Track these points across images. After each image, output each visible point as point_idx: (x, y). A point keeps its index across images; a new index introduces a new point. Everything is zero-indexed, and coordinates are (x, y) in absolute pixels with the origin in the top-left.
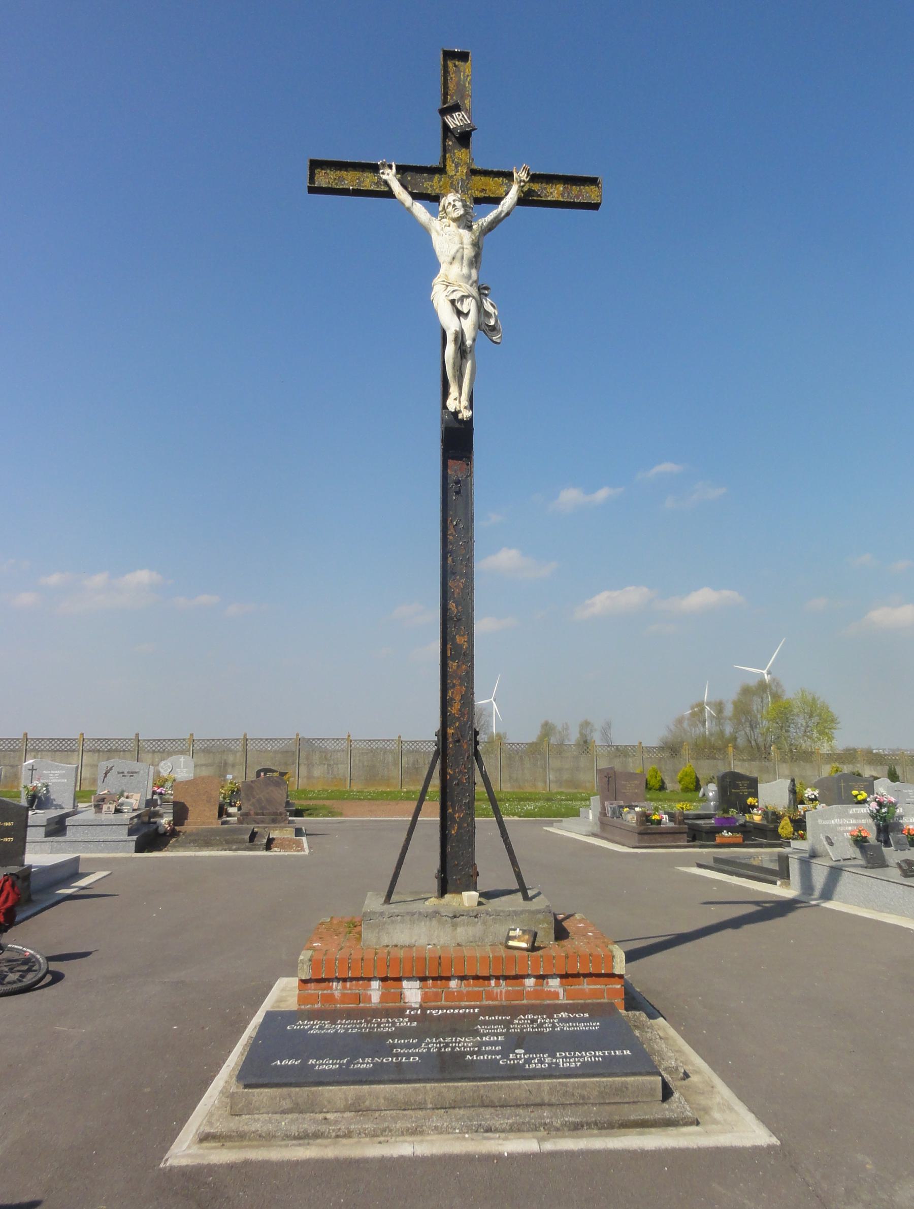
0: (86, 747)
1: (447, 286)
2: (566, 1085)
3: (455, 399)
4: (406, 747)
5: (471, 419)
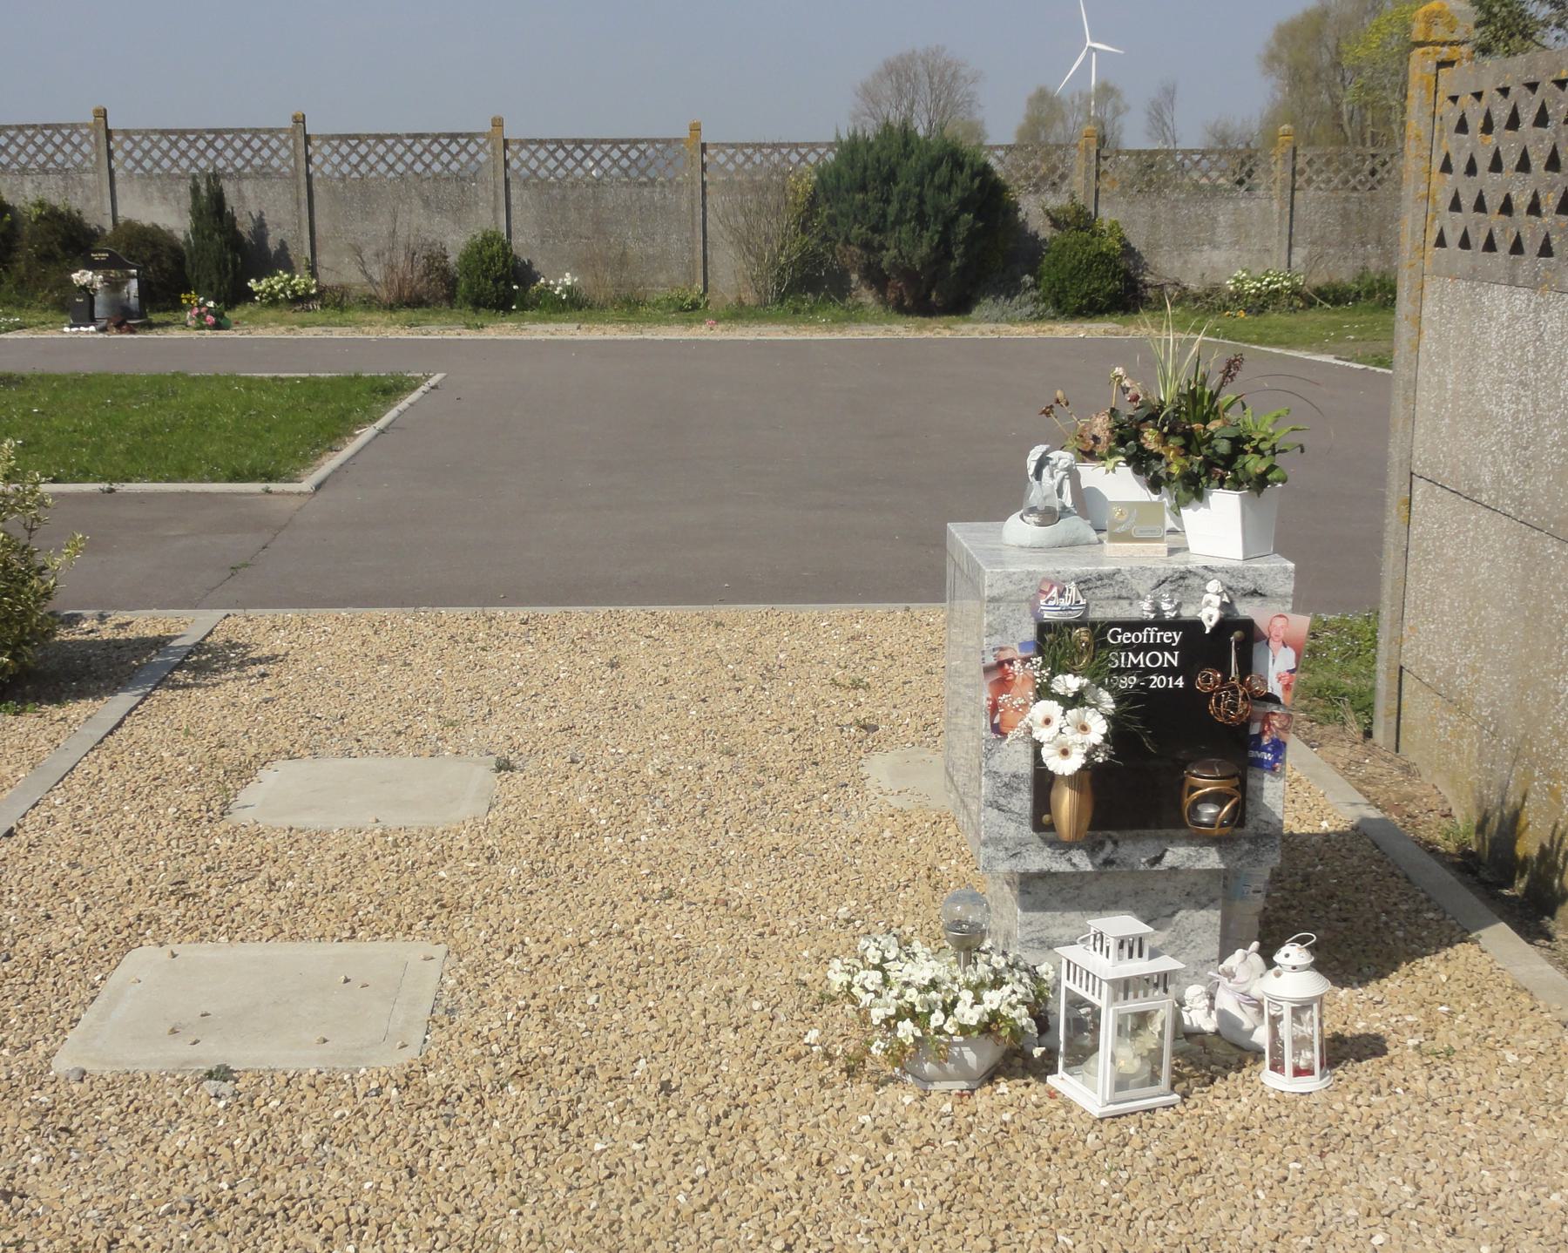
0: (318, 168)
4: (524, 164)
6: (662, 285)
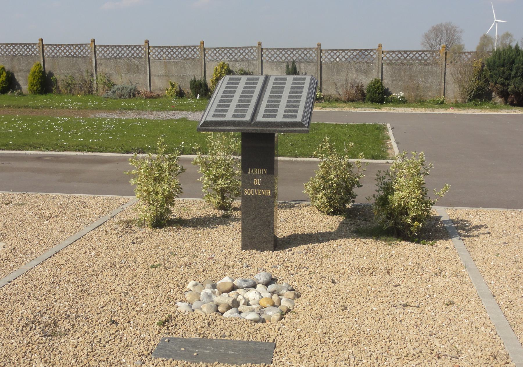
6: (430, 96)
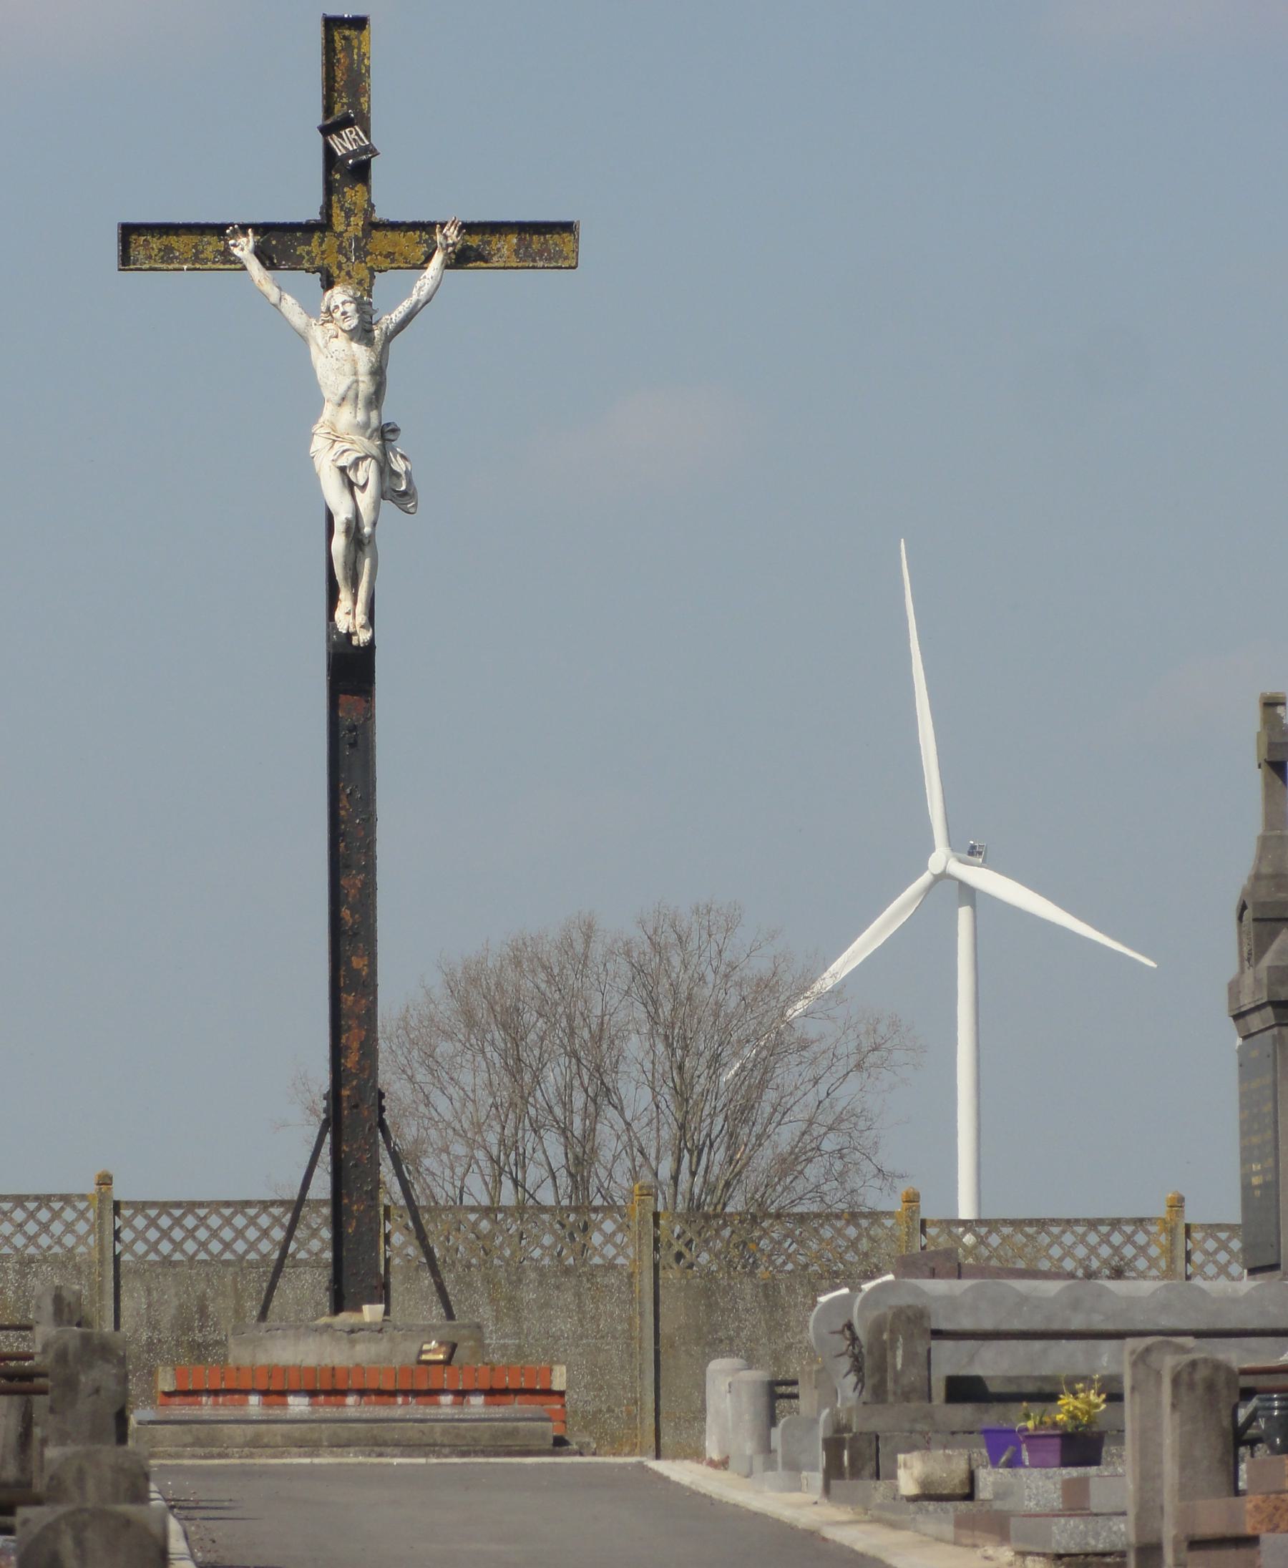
1: (334, 441)
2: (458, 1428)
3: (348, 613)
5: (371, 646)
